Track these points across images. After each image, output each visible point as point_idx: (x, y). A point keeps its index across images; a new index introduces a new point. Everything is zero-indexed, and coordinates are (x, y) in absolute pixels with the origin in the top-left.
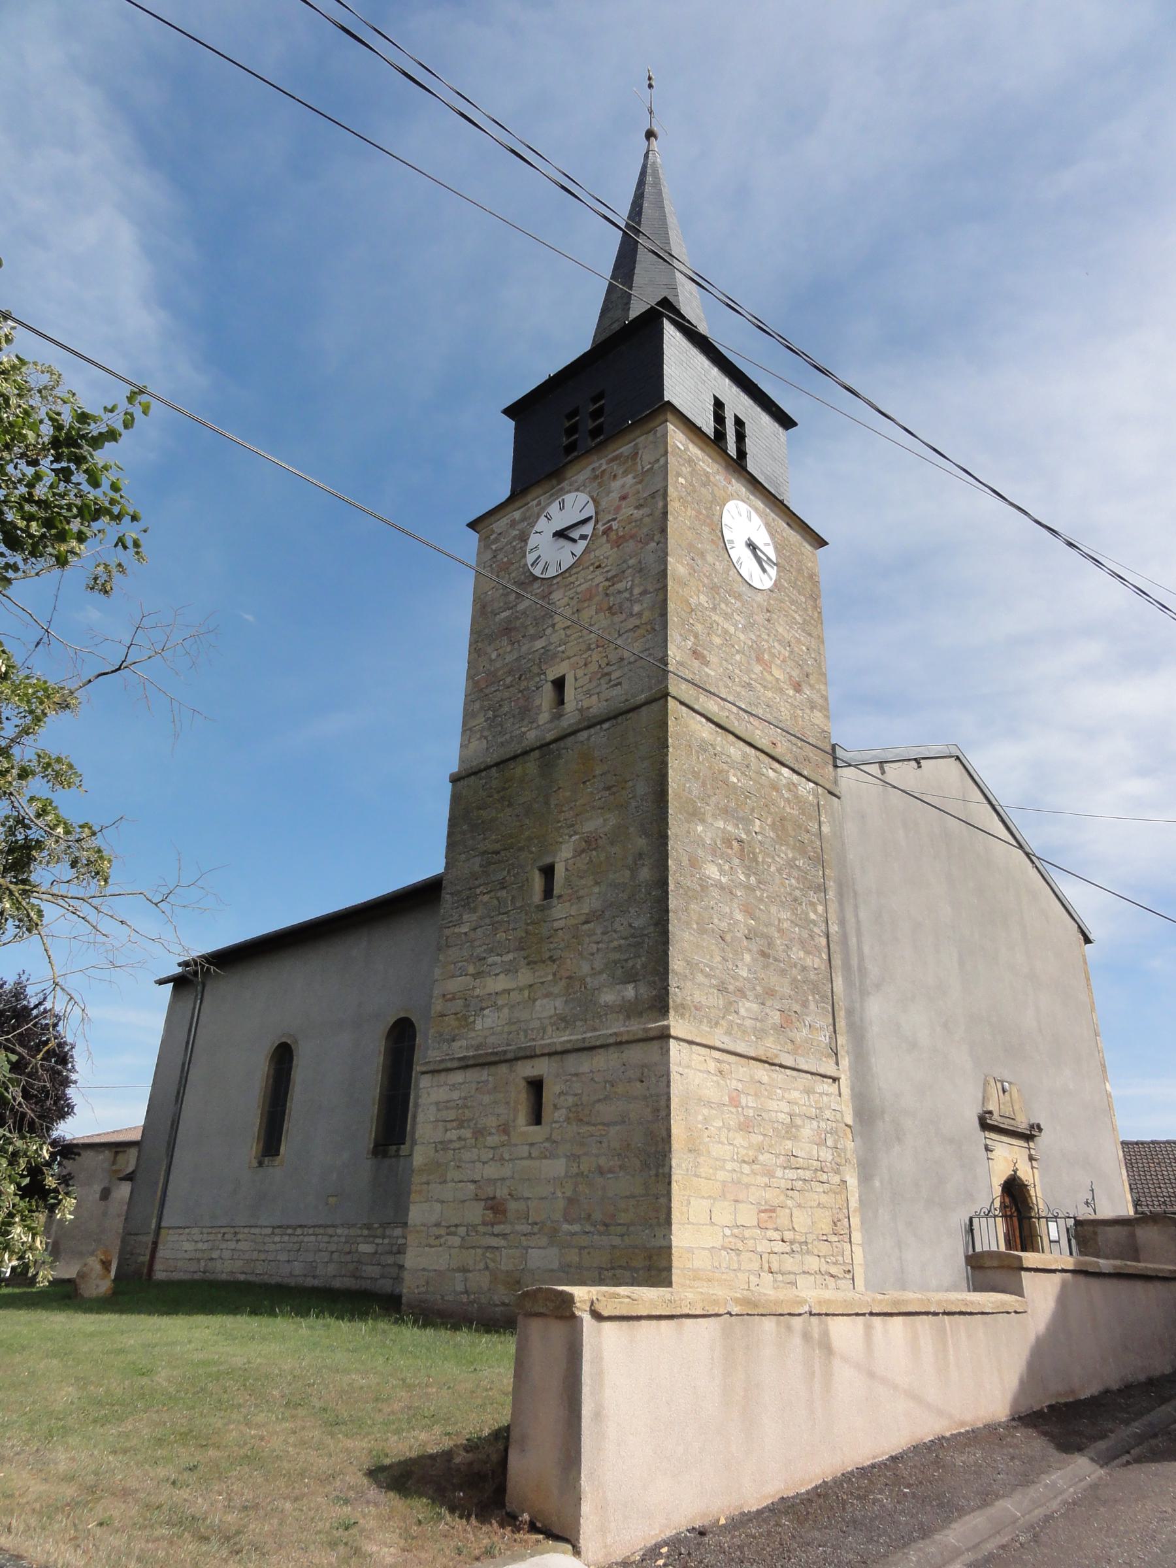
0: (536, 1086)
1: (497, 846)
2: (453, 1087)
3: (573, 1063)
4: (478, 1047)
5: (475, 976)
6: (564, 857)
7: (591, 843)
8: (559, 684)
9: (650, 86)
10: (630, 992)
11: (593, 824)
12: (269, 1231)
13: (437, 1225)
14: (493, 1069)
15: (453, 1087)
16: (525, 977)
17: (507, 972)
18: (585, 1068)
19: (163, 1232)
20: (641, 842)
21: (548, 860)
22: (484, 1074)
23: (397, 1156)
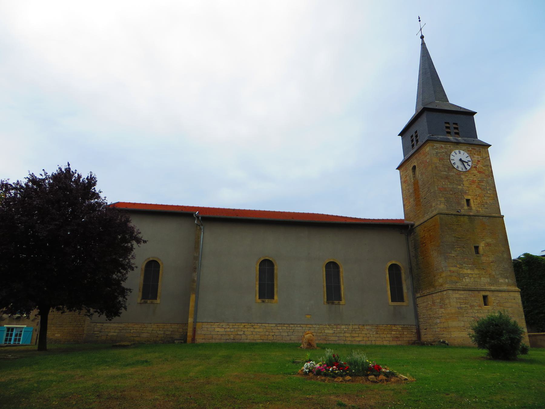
0: (485, 297)
1: (459, 237)
2: (460, 294)
3: (496, 294)
4: (466, 286)
5: (460, 268)
6: (482, 246)
7: (488, 245)
8: (468, 201)
9: (420, 21)
10: (507, 281)
11: (489, 240)
12: (274, 325)
13: (464, 327)
14: (473, 292)
15: (460, 294)
16: (476, 271)
17: (471, 269)
18: (500, 295)
19: (198, 324)
20: (503, 249)
21: (477, 245)
22: (470, 293)
23: (339, 304)
